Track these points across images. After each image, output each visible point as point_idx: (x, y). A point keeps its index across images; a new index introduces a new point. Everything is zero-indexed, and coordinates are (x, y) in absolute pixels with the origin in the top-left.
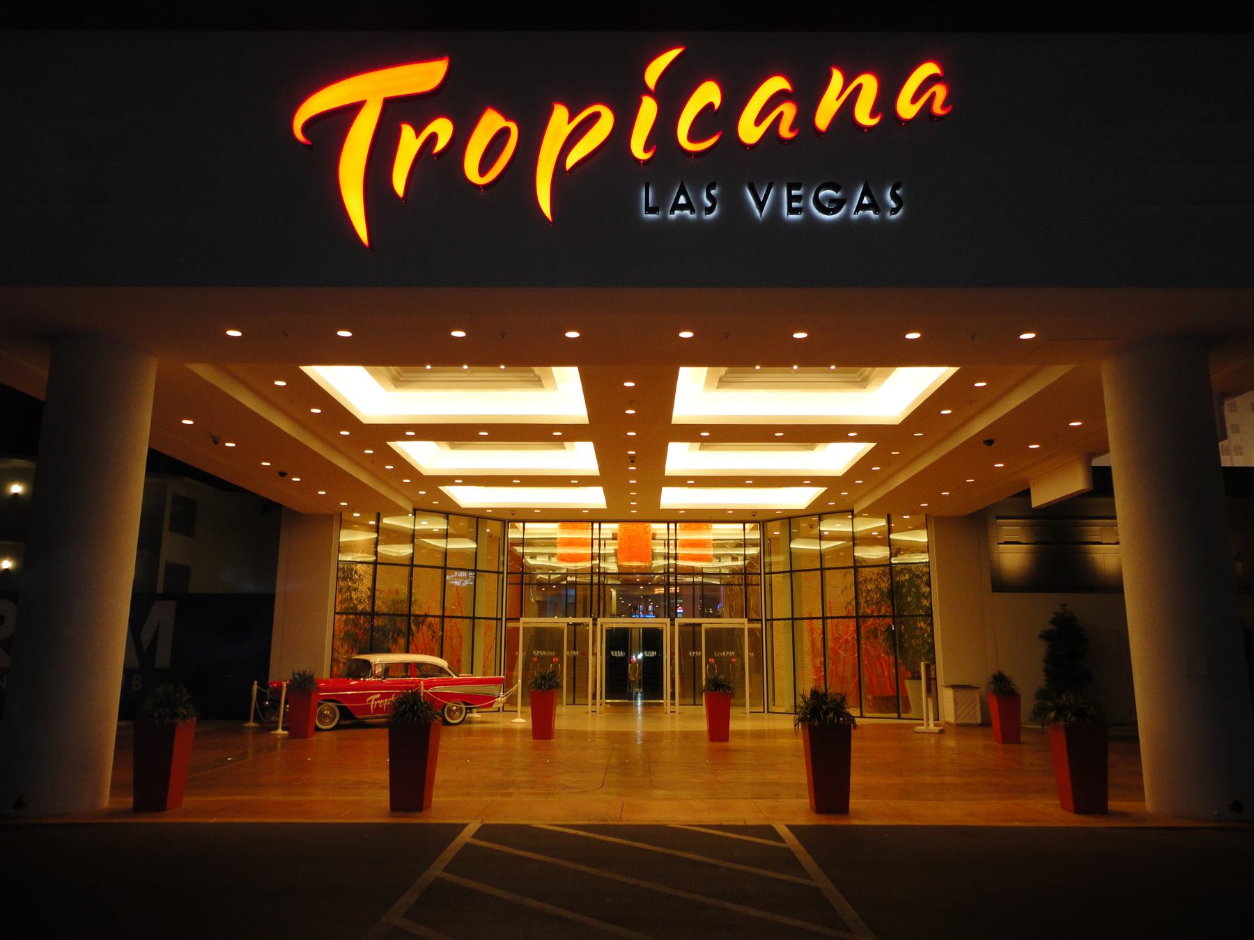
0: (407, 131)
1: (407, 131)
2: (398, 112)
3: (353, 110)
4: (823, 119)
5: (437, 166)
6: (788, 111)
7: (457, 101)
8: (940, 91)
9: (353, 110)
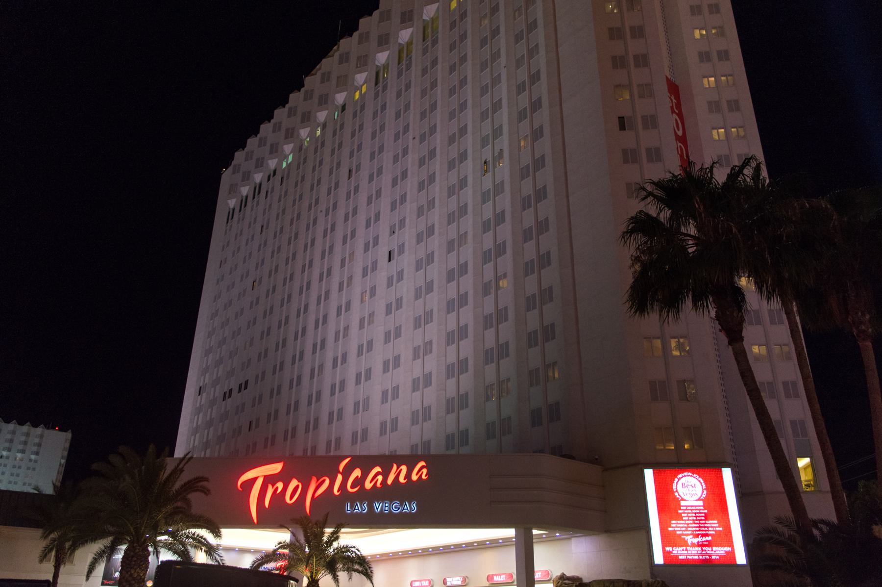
0: (270, 487)
1: (270, 487)
2: (269, 480)
3: (254, 480)
4: (389, 482)
5: (278, 497)
6: (380, 478)
7: (284, 477)
8: (425, 471)
9: (254, 480)
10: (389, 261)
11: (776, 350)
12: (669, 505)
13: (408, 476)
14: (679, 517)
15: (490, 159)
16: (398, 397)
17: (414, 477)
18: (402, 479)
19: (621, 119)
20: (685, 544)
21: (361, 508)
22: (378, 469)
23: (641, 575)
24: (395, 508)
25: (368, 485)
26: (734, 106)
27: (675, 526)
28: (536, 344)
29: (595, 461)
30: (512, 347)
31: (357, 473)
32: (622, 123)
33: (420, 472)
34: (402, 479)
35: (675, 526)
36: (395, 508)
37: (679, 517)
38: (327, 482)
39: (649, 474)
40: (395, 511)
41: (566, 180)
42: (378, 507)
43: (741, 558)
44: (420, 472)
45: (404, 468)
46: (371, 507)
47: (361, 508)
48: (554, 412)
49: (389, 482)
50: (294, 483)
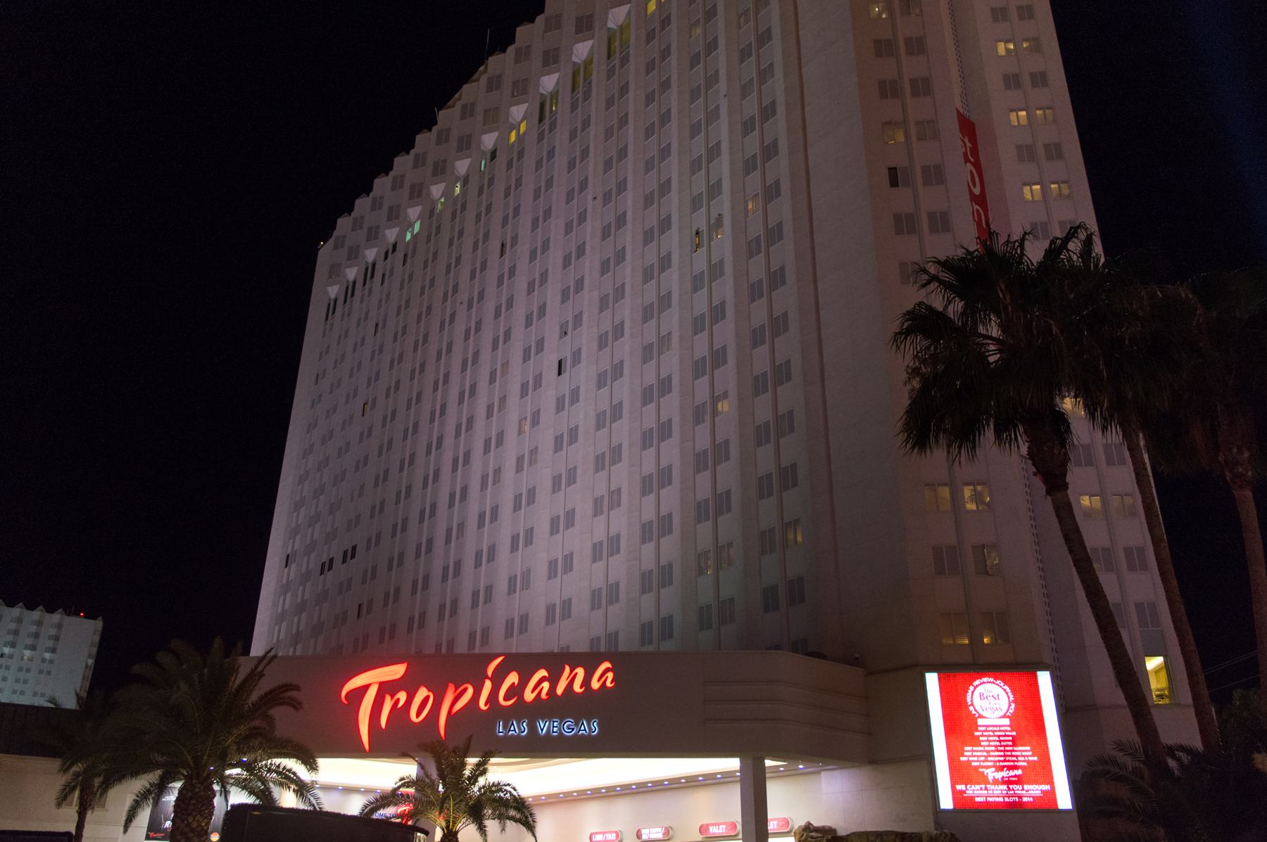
0: (388, 698)
1: (388, 698)
2: (387, 688)
3: (365, 688)
4: (559, 691)
5: (399, 713)
6: (546, 685)
7: (408, 684)
8: (610, 675)
9: (365, 688)
10: (560, 374)
11: (1115, 502)
12: (961, 724)
13: (586, 682)
14: (976, 742)
15: (704, 228)
16: (571, 570)
17: (595, 685)
18: (577, 688)
19: (893, 171)
20: (983, 780)
21: (519, 729)
22: (543, 673)
23: (921, 825)
24: (568, 728)
25: (529, 696)
26: (1054, 151)
27: (970, 754)
28: (770, 494)
29: (855, 662)
30: (736, 498)
31: (513, 678)
32: (894, 177)
33: (603, 678)
34: (577, 688)
35: (970, 754)
36: (568, 728)
37: (976, 742)
38: (470, 691)
39: (932, 680)
40: (568, 733)
41: (814, 258)
42: (543, 727)
43: (1065, 801)
44: (603, 678)
45: (580, 672)
46: (532, 728)
47: (519, 729)
48: (796, 591)
49: (559, 691)
50: (422, 693)
